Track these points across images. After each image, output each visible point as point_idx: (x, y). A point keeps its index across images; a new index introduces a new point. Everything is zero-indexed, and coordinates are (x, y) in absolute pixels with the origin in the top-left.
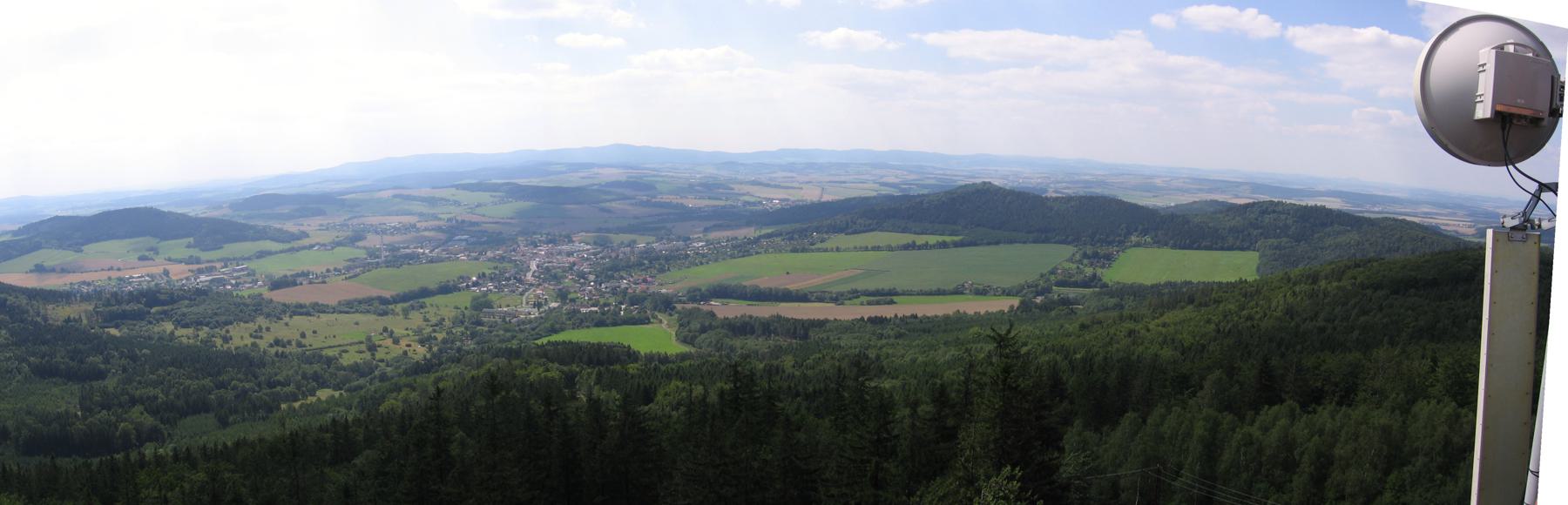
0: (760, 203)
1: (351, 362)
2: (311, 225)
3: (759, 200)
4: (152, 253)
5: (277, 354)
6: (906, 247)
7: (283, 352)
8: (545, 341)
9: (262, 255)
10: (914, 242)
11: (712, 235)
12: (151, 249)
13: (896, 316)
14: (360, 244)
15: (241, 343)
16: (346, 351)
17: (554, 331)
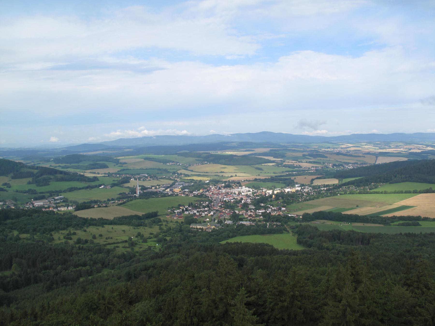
0: (342, 165)
1: (120, 253)
2: (100, 173)
3: (341, 163)
4: (5, 187)
5: (79, 247)
6: (87, 188)
7: (82, 247)
8: (223, 242)
9: (71, 190)
10: (431, 188)
11: (317, 183)
12: (5, 184)
13: (421, 233)
14: (126, 185)
15: (58, 242)
16: (118, 247)
17: (229, 237)
